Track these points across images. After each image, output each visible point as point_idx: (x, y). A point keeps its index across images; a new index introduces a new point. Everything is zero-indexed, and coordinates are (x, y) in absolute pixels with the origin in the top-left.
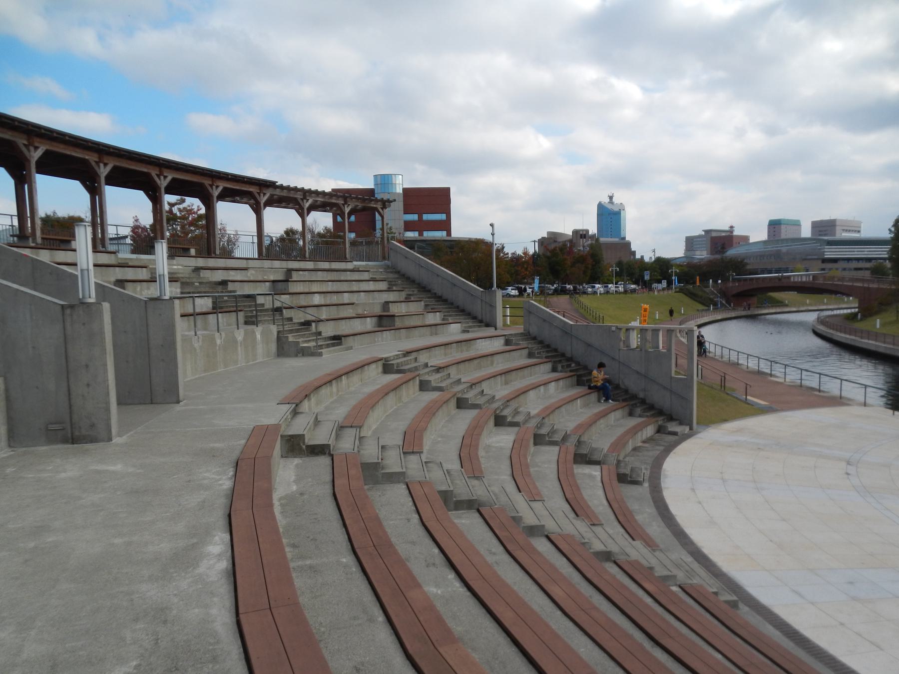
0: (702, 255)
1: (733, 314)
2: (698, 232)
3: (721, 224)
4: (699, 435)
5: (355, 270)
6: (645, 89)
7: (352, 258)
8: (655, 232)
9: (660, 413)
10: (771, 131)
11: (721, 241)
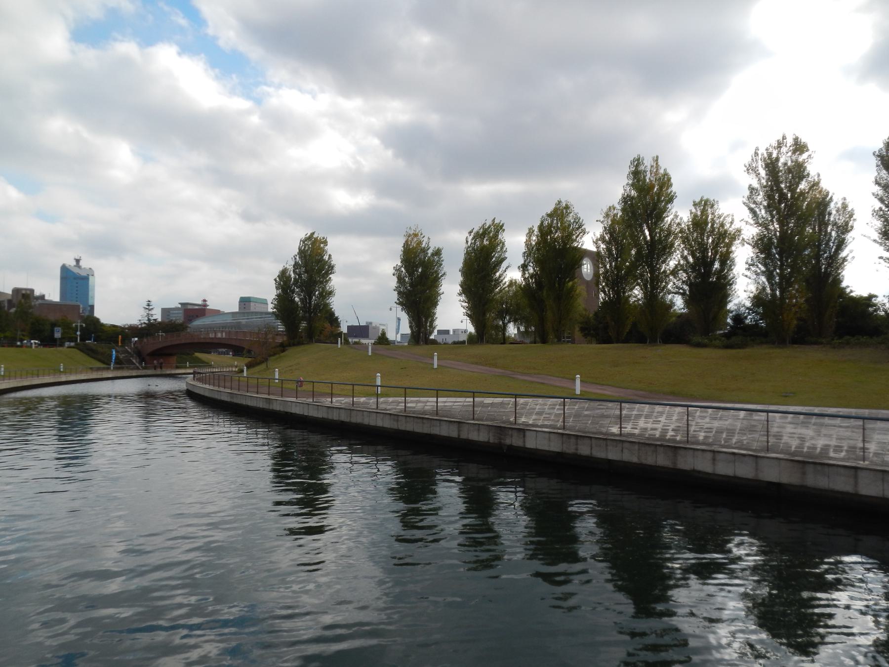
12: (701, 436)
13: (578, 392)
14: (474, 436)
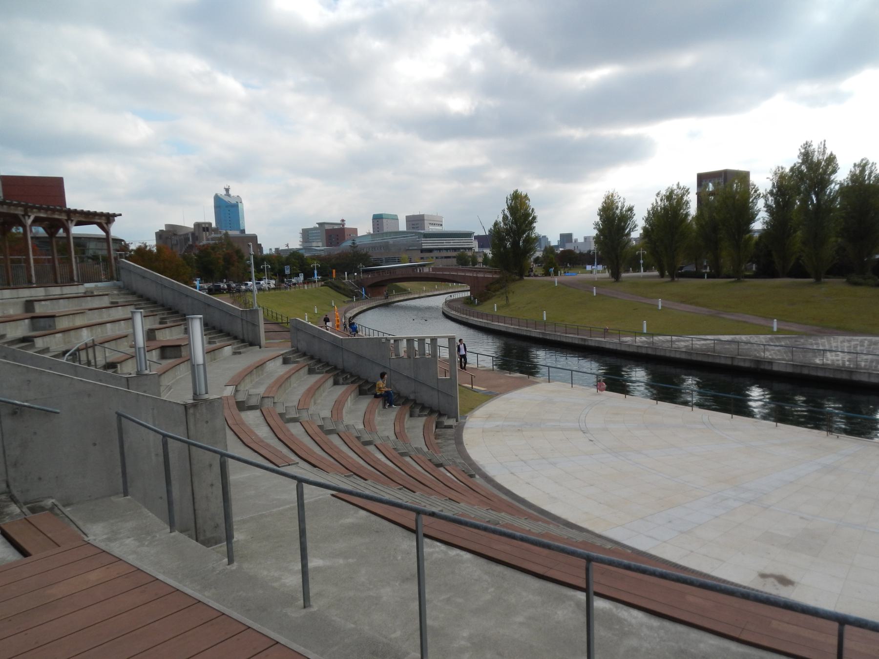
0: (319, 246)
1: (374, 304)
2: (312, 225)
3: (332, 216)
4: (466, 425)
5: (89, 294)
6: (246, 86)
7: (78, 281)
8: (275, 223)
9: (432, 411)
10: (366, 136)
11: (335, 233)
12: (863, 364)
13: (775, 329)
14: (742, 364)
